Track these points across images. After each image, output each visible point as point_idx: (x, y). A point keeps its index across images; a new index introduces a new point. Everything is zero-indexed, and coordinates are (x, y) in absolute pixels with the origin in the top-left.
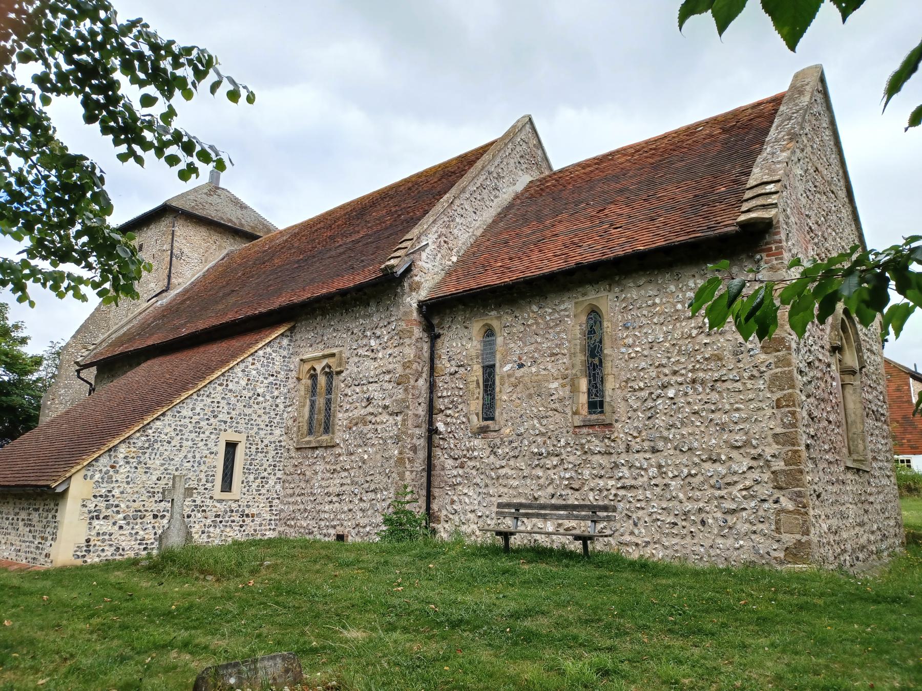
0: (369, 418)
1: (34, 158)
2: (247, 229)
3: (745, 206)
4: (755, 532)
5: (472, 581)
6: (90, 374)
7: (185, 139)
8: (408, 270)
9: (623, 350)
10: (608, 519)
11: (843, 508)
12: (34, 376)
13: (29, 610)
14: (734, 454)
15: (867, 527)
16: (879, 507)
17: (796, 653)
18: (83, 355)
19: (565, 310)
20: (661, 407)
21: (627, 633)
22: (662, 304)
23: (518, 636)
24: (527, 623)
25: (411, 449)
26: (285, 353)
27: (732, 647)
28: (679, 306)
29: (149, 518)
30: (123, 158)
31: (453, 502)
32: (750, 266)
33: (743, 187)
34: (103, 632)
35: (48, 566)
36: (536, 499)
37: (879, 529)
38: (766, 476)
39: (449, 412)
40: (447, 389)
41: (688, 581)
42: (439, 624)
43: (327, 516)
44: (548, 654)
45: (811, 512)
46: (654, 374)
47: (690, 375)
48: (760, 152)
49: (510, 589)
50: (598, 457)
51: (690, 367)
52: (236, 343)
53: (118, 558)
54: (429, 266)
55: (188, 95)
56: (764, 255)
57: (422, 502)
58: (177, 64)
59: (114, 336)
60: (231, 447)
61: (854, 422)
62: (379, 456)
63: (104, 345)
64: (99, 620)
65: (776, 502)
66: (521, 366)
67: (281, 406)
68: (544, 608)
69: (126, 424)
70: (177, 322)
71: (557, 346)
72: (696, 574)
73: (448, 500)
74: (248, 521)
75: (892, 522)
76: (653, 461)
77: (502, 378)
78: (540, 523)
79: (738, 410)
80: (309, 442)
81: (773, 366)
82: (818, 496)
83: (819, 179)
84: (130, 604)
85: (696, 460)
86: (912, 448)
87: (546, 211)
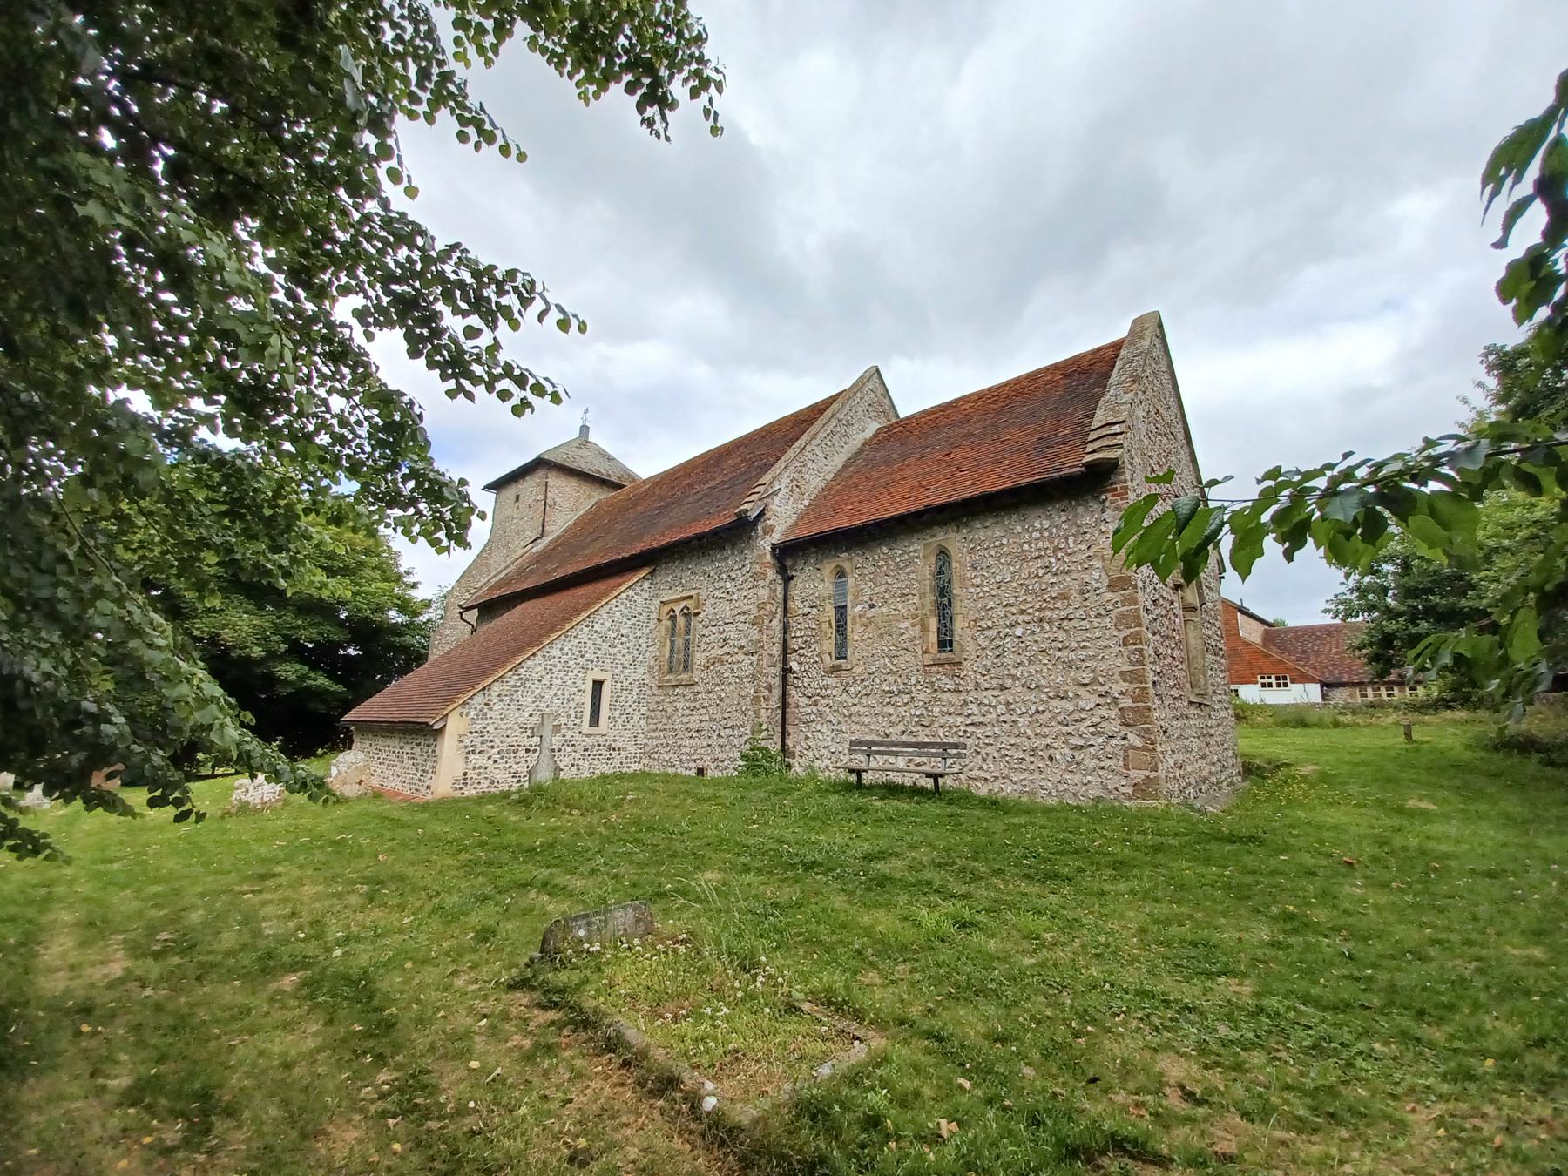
0: (726, 657)
1: (357, 399)
2: (614, 479)
3: (1090, 448)
4: (1103, 768)
5: (825, 819)
6: (473, 616)
7: (517, 372)
8: (762, 514)
9: (972, 590)
10: (959, 756)
11: (1186, 742)
12: (424, 618)
13: (403, 844)
14: (1082, 691)
15: (1208, 760)
16: (1218, 739)
17: (1157, 901)
18: (466, 598)
19: (914, 551)
20: (1009, 645)
21: (982, 878)
22: (1009, 544)
23: (872, 880)
24: (880, 866)
25: (766, 688)
26: (646, 596)
27: (1091, 895)
28: (1026, 547)
29: (522, 752)
30: (451, 394)
31: (807, 738)
32: (1094, 506)
33: (1086, 429)
34: (469, 868)
35: (429, 797)
36: (887, 736)
37: (1219, 760)
38: (1114, 713)
39: (802, 652)
40: (801, 630)
41: (1040, 819)
42: (793, 866)
43: (687, 750)
44: (903, 899)
45: (1159, 749)
46: (1002, 614)
47: (1037, 614)
48: (1102, 395)
49: (863, 827)
50: (948, 694)
51: (1037, 606)
52: (601, 586)
53: (493, 790)
54: (782, 510)
55: (515, 325)
56: (1109, 495)
57: (777, 738)
58: (501, 292)
59: (493, 581)
60: (598, 684)
61: (1195, 658)
62: (735, 694)
63: (485, 589)
64: (468, 856)
65: (1124, 738)
66: (872, 606)
67: (644, 646)
68: (897, 849)
69: (499, 664)
70: (549, 567)
71: (908, 587)
72: (1048, 811)
73: (802, 736)
74: (615, 754)
75: (1230, 753)
76: (1001, 699)
77: (854, 618)
78: (891, 759)
79: (1084, 647)
80: (670, 680)
81: (1119, 605)
82: (1165, 732)
83: (1159, 419)
84: (497, 839)
85: (1044, 697)
86: (1239, 677)
87: (894, 456)
